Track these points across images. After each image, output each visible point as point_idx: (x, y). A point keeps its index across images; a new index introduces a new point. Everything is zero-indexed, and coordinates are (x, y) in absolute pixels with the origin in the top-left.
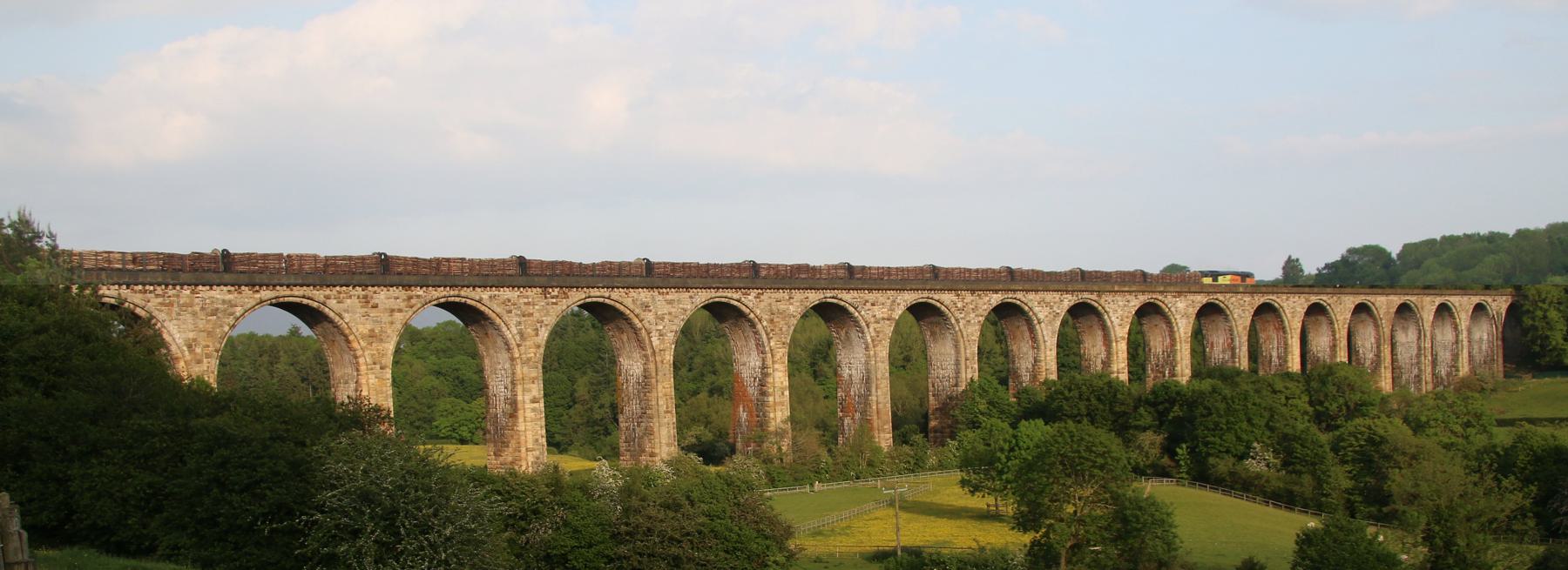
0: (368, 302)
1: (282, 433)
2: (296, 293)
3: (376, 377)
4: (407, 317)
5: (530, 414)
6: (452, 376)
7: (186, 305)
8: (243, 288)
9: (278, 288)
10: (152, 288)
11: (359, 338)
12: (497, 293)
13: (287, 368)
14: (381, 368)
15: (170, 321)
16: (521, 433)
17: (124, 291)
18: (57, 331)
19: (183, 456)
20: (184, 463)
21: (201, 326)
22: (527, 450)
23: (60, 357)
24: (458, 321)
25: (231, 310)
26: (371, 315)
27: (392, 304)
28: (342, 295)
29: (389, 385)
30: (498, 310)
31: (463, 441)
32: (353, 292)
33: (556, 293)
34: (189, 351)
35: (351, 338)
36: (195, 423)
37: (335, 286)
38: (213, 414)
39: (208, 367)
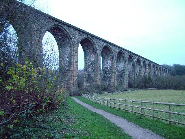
33: (81, 33)
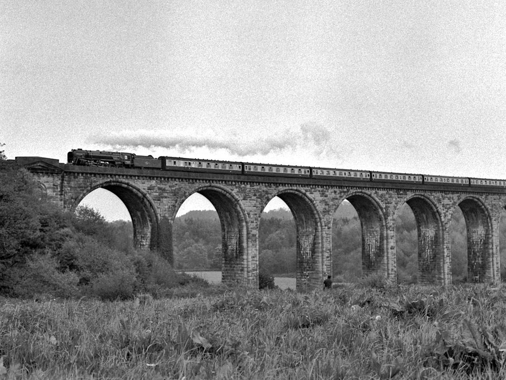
27: (333, 195)
32: (317, 189)
33: (401, 192)
37: (310, 185)
38: (147, 211)
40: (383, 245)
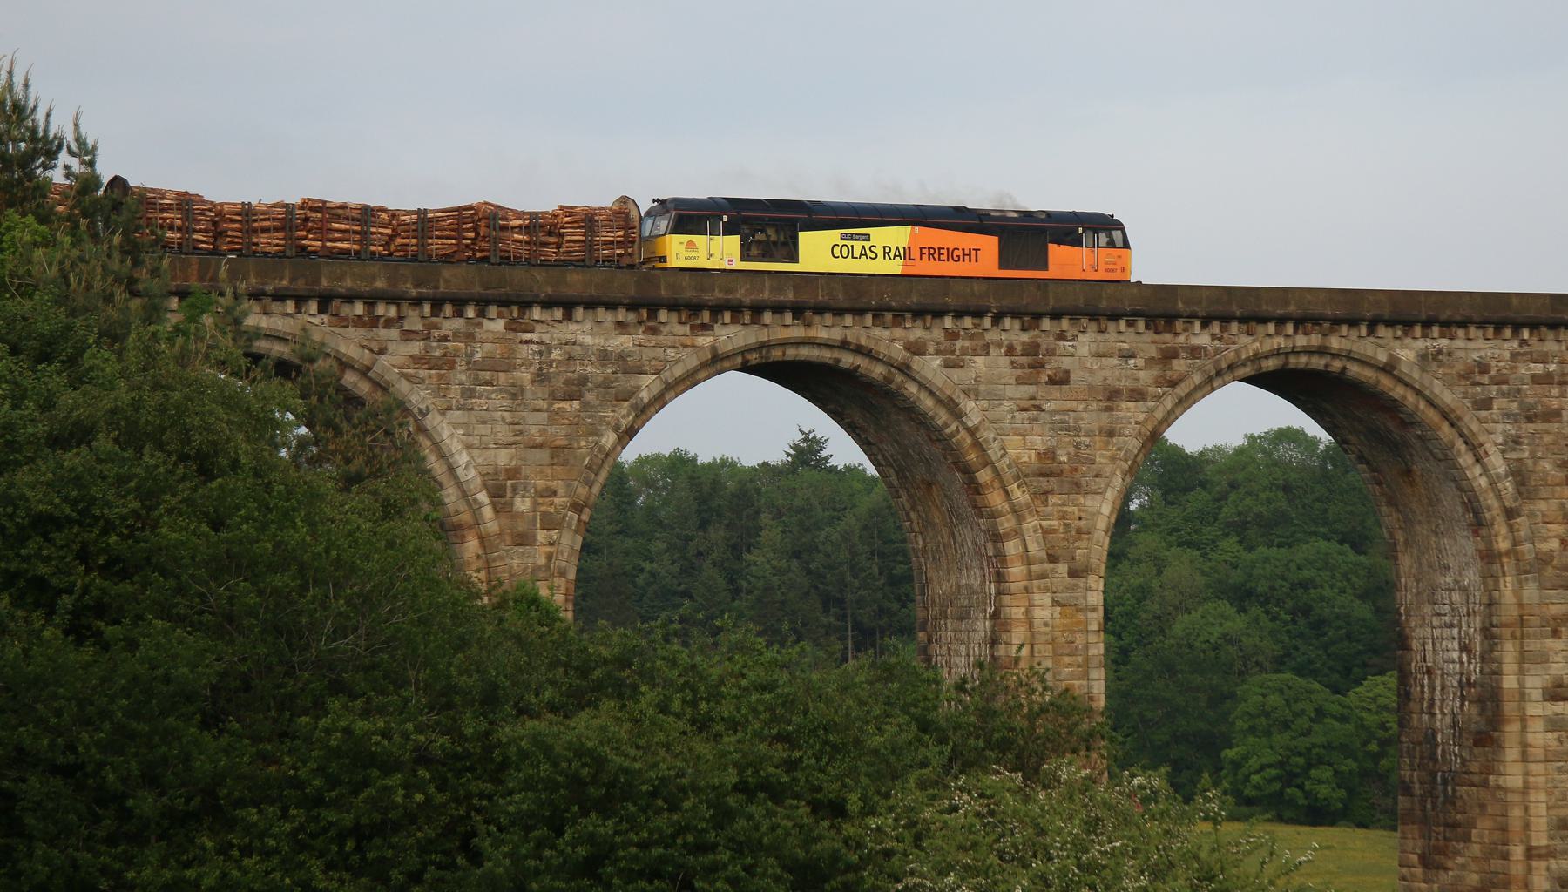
0: (1038, 366)
1: (771, 770)
2: (822, 334)
3: (1055, 603)
4: (1159, 415)
5: (1539, 737)
6: (1289, 604)
7: (492, 365)
8: (663, 315)
9: (767, 317)
10: (392, 312)
11: (1008, 474)
12: (1444, 342)
13: (783, 564)
14: (1073, 574)
15: (443, 412)
16: (1510, 797)
17: (314, 320)
18: (116, 441)
19: (474, 834)
20: (476, 858)
21: (534, 430)
22: (1531, 854)
23: (123, 518)
24: (1313, 429)
25: (624, 382)
26: (1046, 406)
27: (1110, 371)
28: (959, 344)
29: (1094, 626)
30: (1447, 397)
31: (1317, 815)
32: (993, 335)
34: (493, 504)
35: (984, 476)
36: (515, 732)
37: (939, 314)
38: (578, 700)
39: (549, 557)
40: (1498, 673)
